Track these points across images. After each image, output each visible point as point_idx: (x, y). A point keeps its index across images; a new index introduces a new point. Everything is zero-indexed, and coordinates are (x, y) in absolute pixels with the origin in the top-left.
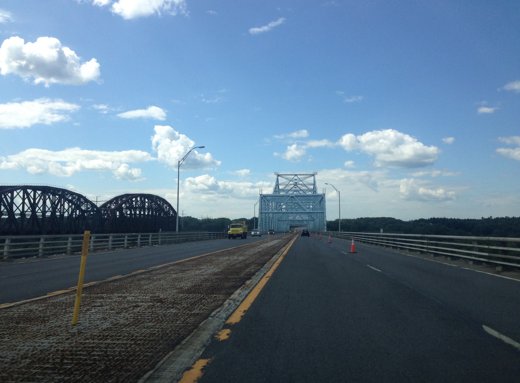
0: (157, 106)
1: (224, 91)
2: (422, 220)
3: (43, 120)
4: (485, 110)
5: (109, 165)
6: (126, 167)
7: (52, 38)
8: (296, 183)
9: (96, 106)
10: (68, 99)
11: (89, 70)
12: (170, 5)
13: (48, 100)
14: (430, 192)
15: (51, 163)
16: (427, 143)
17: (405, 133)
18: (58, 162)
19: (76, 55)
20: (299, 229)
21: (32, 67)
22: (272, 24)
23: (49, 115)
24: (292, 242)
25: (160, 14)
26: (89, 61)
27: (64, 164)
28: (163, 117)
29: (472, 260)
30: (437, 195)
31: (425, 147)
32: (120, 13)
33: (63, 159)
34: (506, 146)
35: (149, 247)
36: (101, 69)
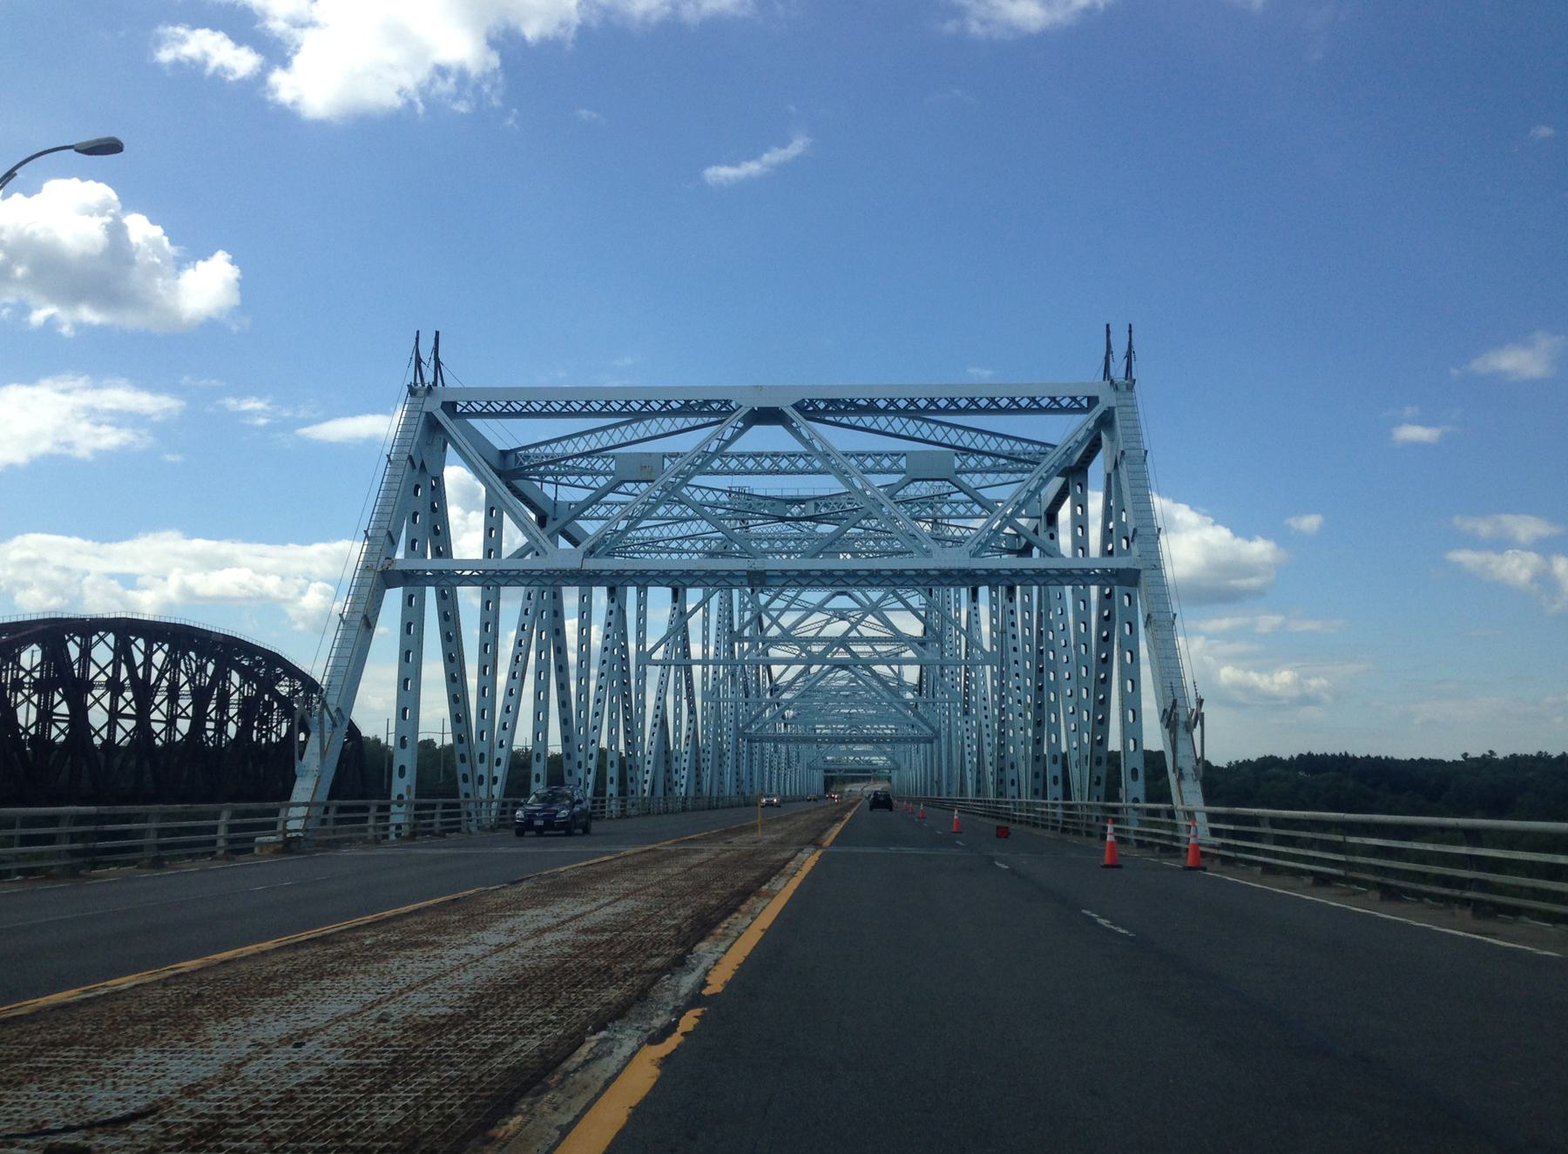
1: (629, 361)
2: (1270, 762)
3: (69, 445)
4: (1413, 433)
5: (271, 584)
6: (324, 593)
7: (91, 182)
9: (231, 403)
10: (143, 383)
11: (207, 286)
12: (451, 80)
13: (81, 382)
14: (1254, 677)
15: (88, 579)
16: (1243, 530)
17: (1176, 501)
18: (111, 576)
19: (166, 239)
20: (856, 788)
21: (20, 271)
22: (774, 156)
23: (85, 427)
25: (421, 107)
27: (129, 581)
29: (1312, 873)
30: (1276, 689)
31: (1239, 542)
32: (294, 103)
33: (129, 568)
34: (1475, 543)
35: (216, 865)
36: (243, 285)
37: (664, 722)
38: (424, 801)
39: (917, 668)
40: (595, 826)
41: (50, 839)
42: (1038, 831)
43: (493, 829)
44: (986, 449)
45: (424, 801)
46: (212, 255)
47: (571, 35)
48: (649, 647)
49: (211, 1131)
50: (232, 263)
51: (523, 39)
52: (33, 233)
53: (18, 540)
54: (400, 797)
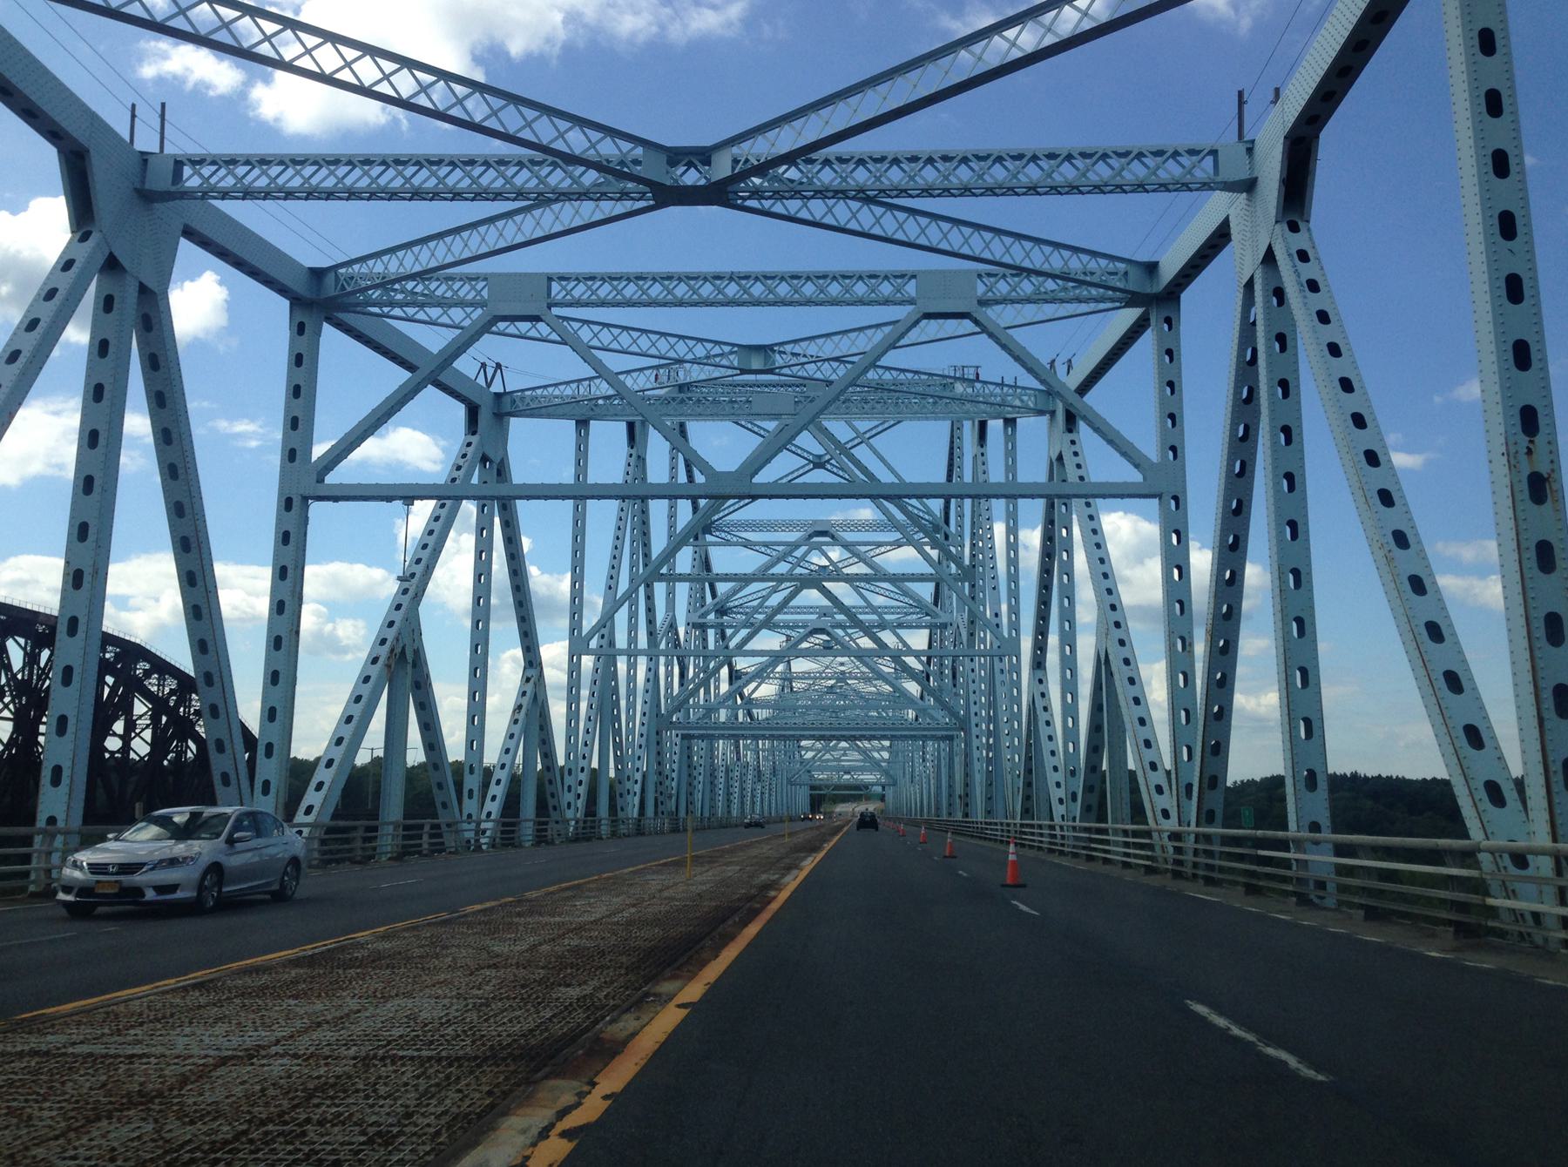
0: (414, 428)
8: (843, 673)
9: (223, 424)
24: (809, 864)
26: (192, 280)
30: (1262, 710)
32: (277, 120)
39: (926, 632)
42: (1057, 860)
43: (576, 839)
44: (1046, 268)
46: (200, 274)
47: (556, 51)
50: (221, 283)
51: (507, 53)
52: (19, 252)
53: (12, 561)
54: (52, 820)
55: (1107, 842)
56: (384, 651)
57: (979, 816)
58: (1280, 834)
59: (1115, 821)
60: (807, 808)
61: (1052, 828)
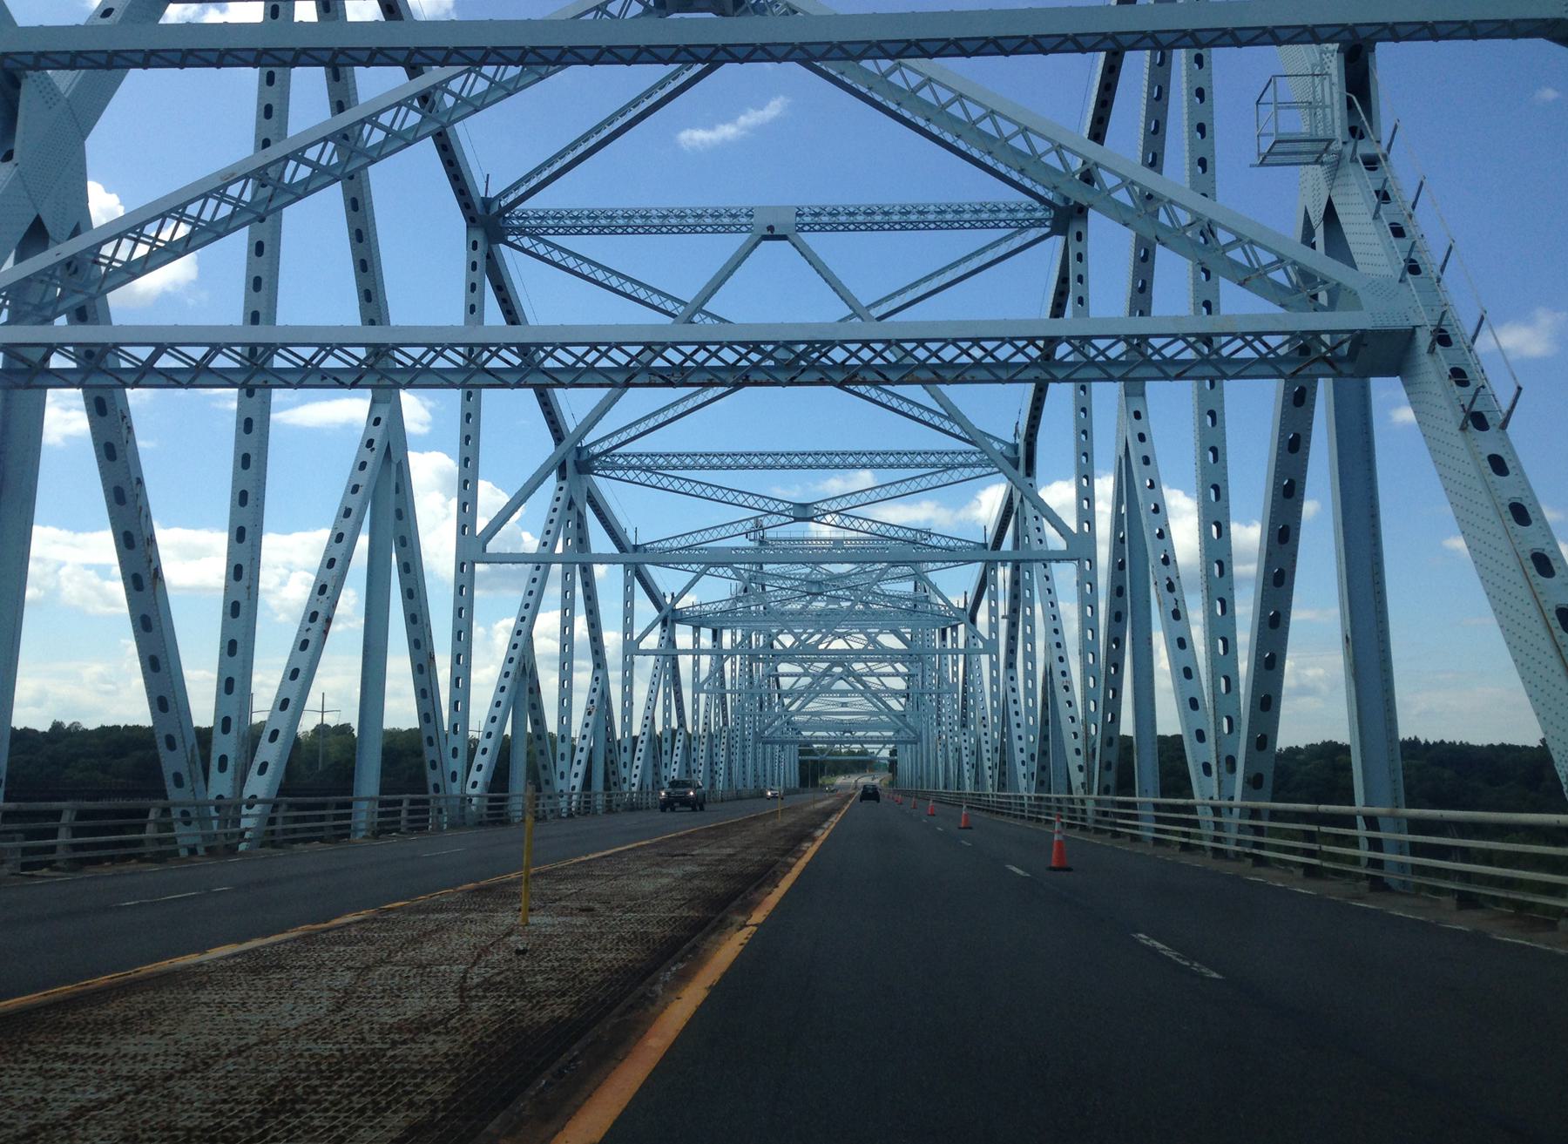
15: (63, 572)
18: (88, 567)
22: (751, 118)
28: (422, 424)
37: (605, 697)
38: (390, 797)
40: (706, 807)
41: (322, 818)
45: (390, 797)
48: (637, 634)
49: (280, 1103)
55: (1136, 817)
56: (512, 668)
57: (968, 788)
58: (1190, 801)
59: (1144, 793)
60: (793, 779)
61: (1072, 801)
